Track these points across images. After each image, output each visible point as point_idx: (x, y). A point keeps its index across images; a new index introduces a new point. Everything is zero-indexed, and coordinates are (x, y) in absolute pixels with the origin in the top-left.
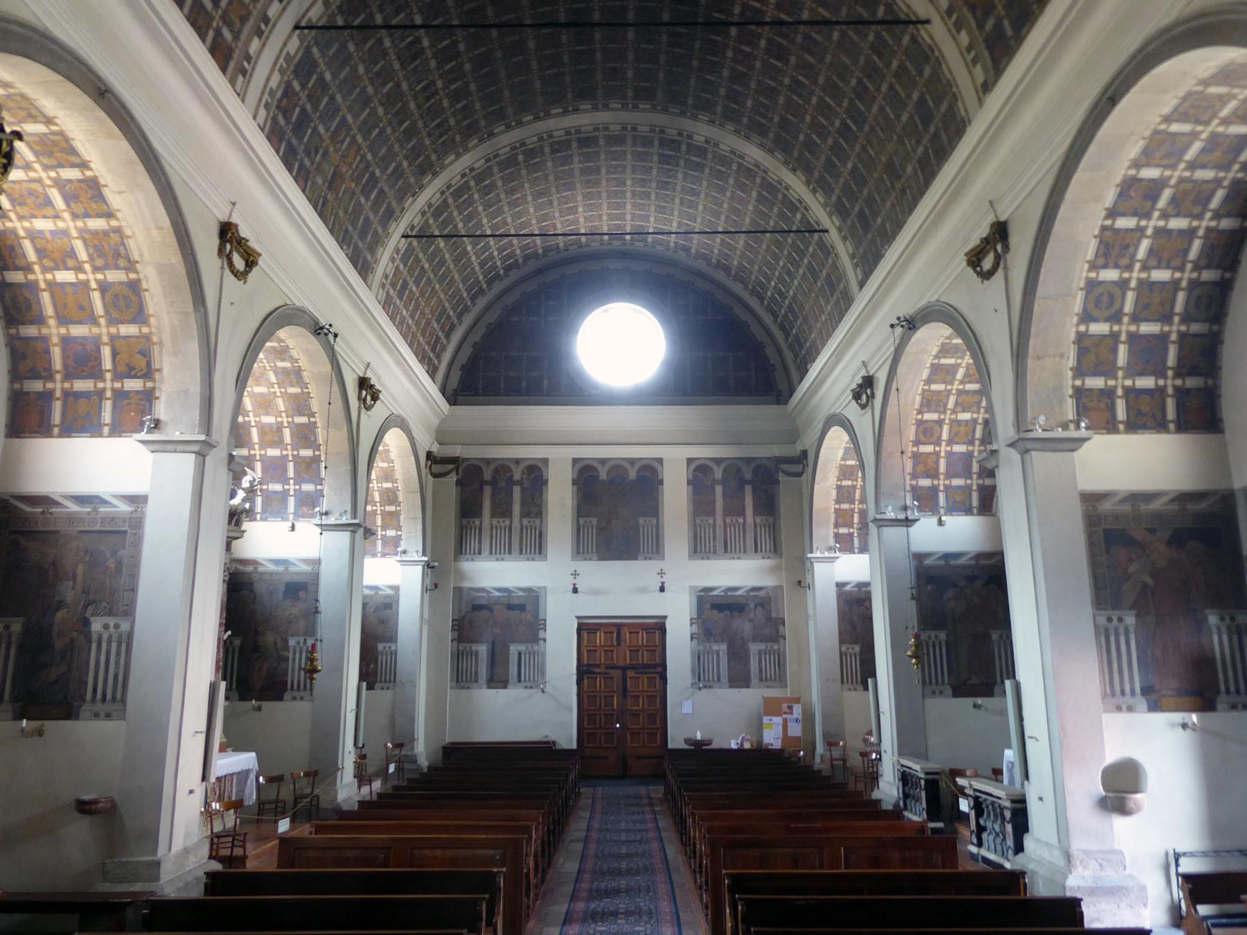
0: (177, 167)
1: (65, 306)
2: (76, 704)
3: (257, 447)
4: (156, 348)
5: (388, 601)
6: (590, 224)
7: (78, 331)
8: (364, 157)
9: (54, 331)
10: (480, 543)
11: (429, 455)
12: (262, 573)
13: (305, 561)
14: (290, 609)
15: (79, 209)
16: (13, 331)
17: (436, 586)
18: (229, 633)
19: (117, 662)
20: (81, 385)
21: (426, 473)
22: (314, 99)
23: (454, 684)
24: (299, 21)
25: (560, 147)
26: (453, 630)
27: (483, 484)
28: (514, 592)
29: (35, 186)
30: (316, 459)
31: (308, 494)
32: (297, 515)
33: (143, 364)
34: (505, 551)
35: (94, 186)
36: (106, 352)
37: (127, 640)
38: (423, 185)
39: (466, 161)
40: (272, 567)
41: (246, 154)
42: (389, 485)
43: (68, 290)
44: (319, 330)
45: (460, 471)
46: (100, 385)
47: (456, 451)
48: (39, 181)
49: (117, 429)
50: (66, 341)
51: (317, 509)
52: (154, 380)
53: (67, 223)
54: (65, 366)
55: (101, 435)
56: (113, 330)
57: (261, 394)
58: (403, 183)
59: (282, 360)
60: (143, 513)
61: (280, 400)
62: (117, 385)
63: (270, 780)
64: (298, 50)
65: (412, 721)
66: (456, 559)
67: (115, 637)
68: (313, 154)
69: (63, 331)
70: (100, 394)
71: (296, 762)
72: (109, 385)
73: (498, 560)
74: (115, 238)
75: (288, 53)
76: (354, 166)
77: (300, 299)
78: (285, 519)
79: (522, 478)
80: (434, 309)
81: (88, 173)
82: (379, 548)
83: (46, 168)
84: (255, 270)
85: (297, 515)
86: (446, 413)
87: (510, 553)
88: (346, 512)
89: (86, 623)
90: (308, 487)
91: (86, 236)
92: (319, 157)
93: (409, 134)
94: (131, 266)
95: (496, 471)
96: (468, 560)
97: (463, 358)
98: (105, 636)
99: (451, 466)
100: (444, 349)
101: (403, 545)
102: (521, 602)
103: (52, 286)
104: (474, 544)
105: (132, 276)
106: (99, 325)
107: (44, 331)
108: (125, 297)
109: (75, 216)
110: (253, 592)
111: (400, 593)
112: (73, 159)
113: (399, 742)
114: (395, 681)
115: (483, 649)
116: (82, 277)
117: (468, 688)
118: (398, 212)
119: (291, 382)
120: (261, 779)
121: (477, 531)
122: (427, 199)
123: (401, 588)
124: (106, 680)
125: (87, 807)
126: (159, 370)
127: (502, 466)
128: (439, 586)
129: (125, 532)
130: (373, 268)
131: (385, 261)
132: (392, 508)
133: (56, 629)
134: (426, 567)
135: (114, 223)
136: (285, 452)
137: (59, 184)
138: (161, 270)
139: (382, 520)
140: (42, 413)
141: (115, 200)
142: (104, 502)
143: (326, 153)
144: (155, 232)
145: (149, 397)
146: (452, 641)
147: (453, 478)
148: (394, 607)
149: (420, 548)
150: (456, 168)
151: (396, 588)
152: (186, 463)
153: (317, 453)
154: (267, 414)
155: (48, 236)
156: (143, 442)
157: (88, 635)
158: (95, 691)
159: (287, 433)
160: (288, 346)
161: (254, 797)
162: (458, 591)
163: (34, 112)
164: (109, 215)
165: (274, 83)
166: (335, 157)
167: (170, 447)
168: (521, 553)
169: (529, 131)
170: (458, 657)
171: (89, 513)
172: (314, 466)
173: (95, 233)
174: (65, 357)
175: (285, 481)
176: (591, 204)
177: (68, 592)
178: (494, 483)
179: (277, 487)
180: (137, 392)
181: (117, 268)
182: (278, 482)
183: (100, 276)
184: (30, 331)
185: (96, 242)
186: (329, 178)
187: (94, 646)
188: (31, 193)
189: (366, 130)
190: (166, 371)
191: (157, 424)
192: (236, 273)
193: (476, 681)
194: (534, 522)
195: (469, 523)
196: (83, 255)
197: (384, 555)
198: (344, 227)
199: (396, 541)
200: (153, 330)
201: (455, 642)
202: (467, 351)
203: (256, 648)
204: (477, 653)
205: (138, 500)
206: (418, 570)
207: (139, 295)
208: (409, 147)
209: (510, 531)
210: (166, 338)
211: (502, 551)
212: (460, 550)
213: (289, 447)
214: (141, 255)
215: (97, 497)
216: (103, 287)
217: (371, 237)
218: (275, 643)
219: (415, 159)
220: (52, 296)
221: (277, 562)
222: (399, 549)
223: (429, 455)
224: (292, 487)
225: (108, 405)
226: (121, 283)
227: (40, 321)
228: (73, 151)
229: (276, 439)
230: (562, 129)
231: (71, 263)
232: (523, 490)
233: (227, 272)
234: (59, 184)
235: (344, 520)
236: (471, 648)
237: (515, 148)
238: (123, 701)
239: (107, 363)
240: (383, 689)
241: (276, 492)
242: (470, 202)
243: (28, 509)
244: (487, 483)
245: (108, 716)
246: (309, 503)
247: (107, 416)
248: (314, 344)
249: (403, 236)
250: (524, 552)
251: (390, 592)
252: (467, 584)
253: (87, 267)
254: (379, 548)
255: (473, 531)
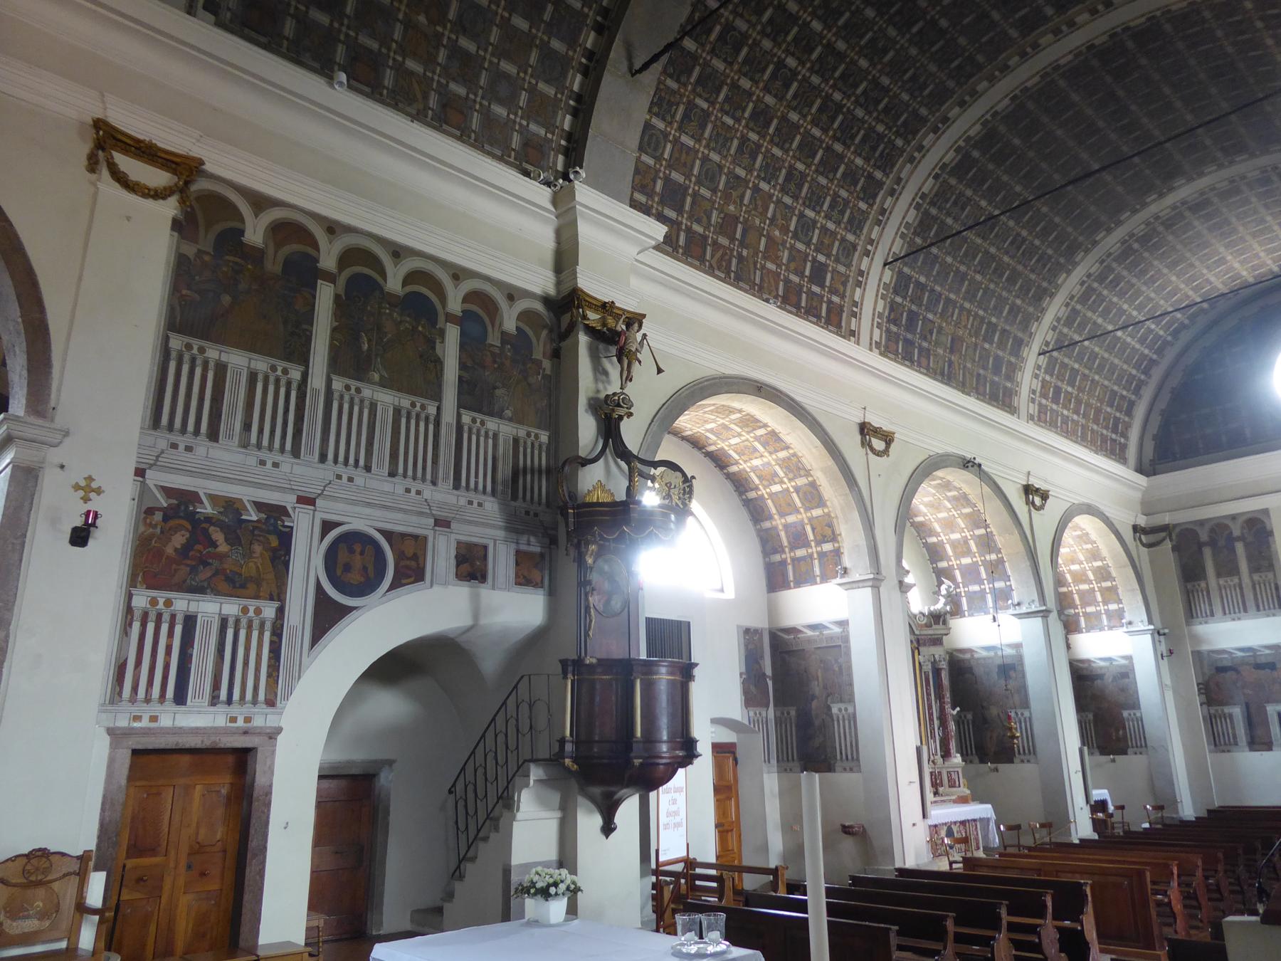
0: (814, 404)
1: (780, 505)
2: (832, 762)
3: (952, 558)
4: (835, 520)
5: (1123, 670)
6: (1250, 265)
7: (791, 519)
8: (976, 315)
9: (779, 522)
10: (1210, 605)
11: (1136, 528)
12: (978, 659)
13: (1010, 646)
14: (999, 684)
15: (772, 449)
16: (758, 527)
17: (1171, 652)
18: (958, 709)
19: (850, 733)
20: (800, 553)
21: (1137, 546)
22: (916, 300)
23: (1213, 747)
24: (886, 260)
25: (1170, 223)
26: (1200, 693)
27: (1200, 545)
28: (1260, 651)
29: (746, 443)
30: (1001, 561)
31: (1001, 590)
32: (996, 609)
33: (830, 532)
34: (1239, 608)
35: (773, 434)
36: (808, 529)
37: (853, 718)
38: (1043, 309)
39: (1079, 273)
40: (984, 654)
41: (864, 369)
42: (1099, 564)
43: (780, 496)
44: (968, 464)
45: (1174, 537)
46: (810, 551)
47: (1166, 519)
48: (747, 440)
49: (825, 578)
50: (786, 526)
51: (1010, 602)
52: (838, 542)
53: (768, 458)
54: (789, 542)
55: (816, 583)
56: (809, 515)
57: (944, 519)
58: (1022, 316)
59: (950, 491)
60: (848, 632)
61: (959, 519)
62: (819, 549)
63: (1009, 828)
64: (892, 277)
65: (1171, 783)
66: (1188, 624)
67: (846, 717)
68: (929, 336)
69: (783, 521)
70: (811, 556)
71: (1033, 816)
72: (814, 550)
73: (1234, 620)
74: (794, 459)
75: (876, 342)
76: (969, 327)
77: (940, 448)
78: (987, 613)
79: (1242, 534)
80: (1101, 396)
81: (769, 429)
82: (1105, 622)
83: (748, 433)
84: (893, 445)
85: (996, 609)
86: (1145, 485)
87: (1245, 611)
88: (1033, 601)
89: (829, 708)
90: (999, 585)
91: (780, 463)
92: (934, 335)
93: (1012, 280)
94: (808, 473)
95: (1212, 530)
96: (1201, 623)
97: (1154, 428)
98: (756, 720)
99: (1163, 534)
100: (1128, 426)
101: (1128, 617)
102: (1270, 660)
103: (771, 495)
104: (1205, 607)
105: (810, 479)
106: (801, 513)
107: (774, 523)
108: (811, 493)
109: (771, 453)
110: (973, 674)
111: (1134, 662)
112: (758, 424)
113: (1162, 804)
114: (1146, 746)
115: (1237, 712)
116: (784, 486)
117: (1229, 751)
118: (1026, 339)
119: (962, 505)
120: (1002, 827)
121: (1205, 593)
122: (1034, 362)
123: (1133, 657)
124: (846, 745)
125: (847, 830)
126: (840, 535)
127: (1219, 525)
128: (1175, 652)
129: (840, 646)
130: (1017, 391)
131: (1027, 381)
132: (1108, 584)
133: (813, 713)
134: (1156, 635)
135: (791, 451)
136: (974, 559)
137: (757, 439)
138: (824, 470)
139: (1102, 595)
140: (783, 575)
141: (788, 439)
142: (825, 627)
143: (940, 329)
144: (814, 450)
145: (837, 553)
146: (1201, 705)
147: (1168, 545)
148: (1131, 676)
149: (1145, 617)
150: (1071, 283)
151: (1129, 658)
152: (866, 594)
153: (1000, 556)
154: (953, 532)
155: (761, 468)
156: (840, 585)
157: (831, 716)
158: (841, 753)
159: (972, 543)
160: (949, 481)
161: (997, 840)
162: (1198, 655)
163: (731, 410)
164: (787, 448)
165: (880, 308)
166: (949, 329)
167: (854, 585)
168: (1258, 609)
169: (1134, 223)
170: (1211, 720)
171: (818, 636)
172: (1000, 566)
173: (784, 460)
174: (788, 537)
175: (981, 582)
176: (1238, 250)
177: (816, 688)
178: (1213, 543)
179: (976, 588)
180: (831, 551)
181: (801, 476)
182: (975, 583)
183: (793, 484)
184: (767, 525)
185: (785, 464)
186: (949, 345)
187: (836, 723)
188: (746, 447)
189: (970, 296)
190: (843, 534)
191: (845, 571)
192: (878, 454)
193: (1236, 744)
194: (1266, 576)
195: (1194, 586)
196: (781, 474)
197: (1111, 628)
198: (975, 373)
199: (1120, 614)
200: (831, 509)
201: (1205, 706)
202: (1156, 420)
203: (985, 721)
204: (1231, 716)
205: (843, 624)
206: (1147, 639)
207: (817, 490)
208: (1017, 288)
209: (1241, 588)
210: (840, 515)
211: (1237, 610)
212: (1191, 615)
213: (977, 555)
214: (811, 465)
215: (821, 624)
216: (797, 490)
217: (1006, 368)
218: (999, 715)
219: (1027, 294)
220: (773, 502)
221: (988, 649)
222: (1124, 621)
223: (1136, 528)
224: (987, 586)
225: (816, 562)
226: (805, 485)
227: (770, 517)
228: (758, 421)
229: (965, 550)
230: (1167, 207)
231: (776, 480)
232: (1247, 546)
233: (871, 455)
234: (757, 439)
235: (1034, 608)
236: (1223, 711)
237: (1126, 241)
238: (858, 760)
239: (811, 537)
240: (1136, 753)
241: (975, 592)
242: (1101, 299)
243: (786, 637)
244: (1206, 544)
245: (851, 770)
246: (1002, 597)
247: (817, 571)
248: (966, 475)
249: (1040, 354)
250: (1261, 608)
251: (1123, 662)
252: (1205, 647)
253: (785, 480)
254: (1105, 622)
255: (1196, 595)
